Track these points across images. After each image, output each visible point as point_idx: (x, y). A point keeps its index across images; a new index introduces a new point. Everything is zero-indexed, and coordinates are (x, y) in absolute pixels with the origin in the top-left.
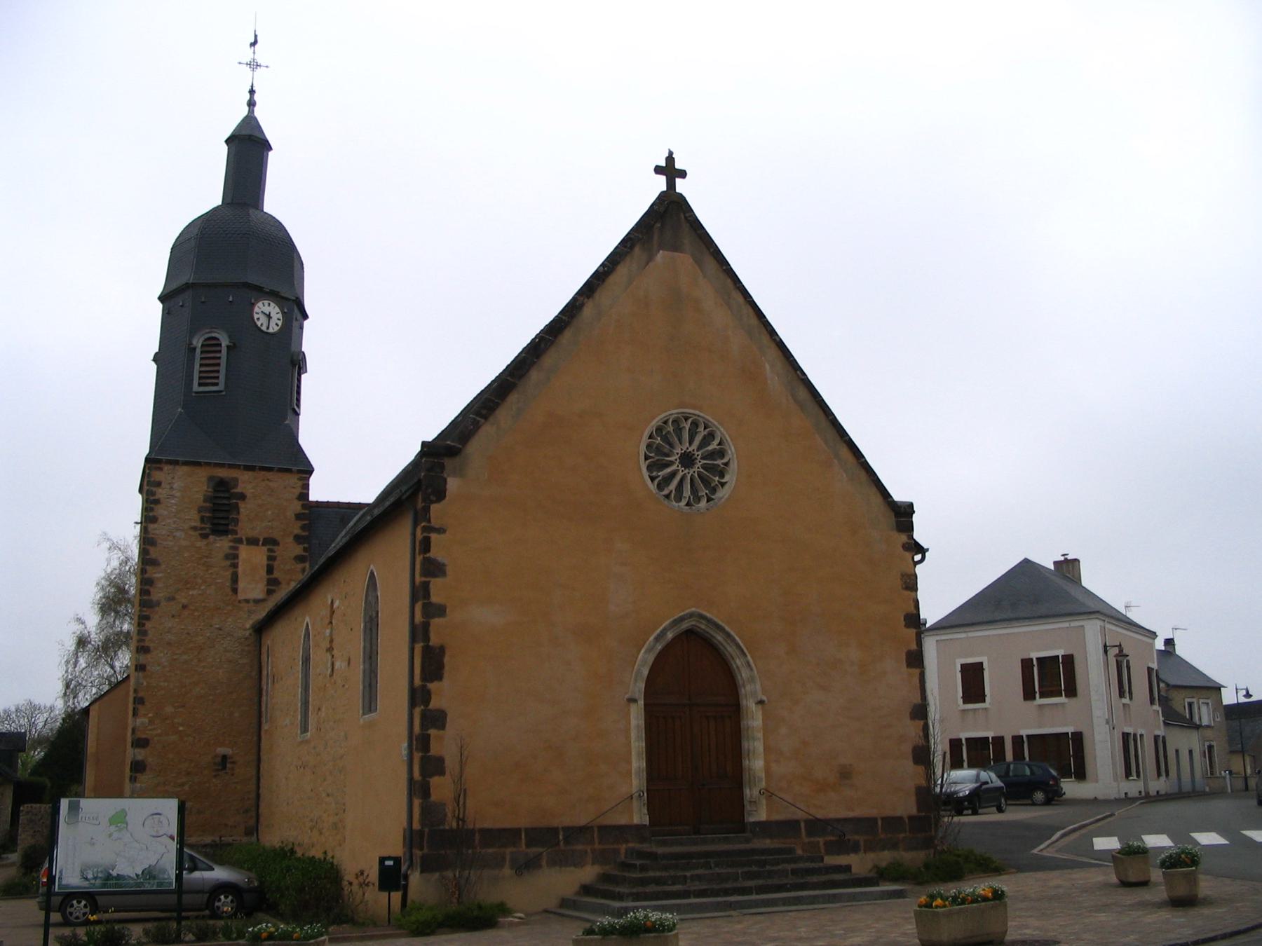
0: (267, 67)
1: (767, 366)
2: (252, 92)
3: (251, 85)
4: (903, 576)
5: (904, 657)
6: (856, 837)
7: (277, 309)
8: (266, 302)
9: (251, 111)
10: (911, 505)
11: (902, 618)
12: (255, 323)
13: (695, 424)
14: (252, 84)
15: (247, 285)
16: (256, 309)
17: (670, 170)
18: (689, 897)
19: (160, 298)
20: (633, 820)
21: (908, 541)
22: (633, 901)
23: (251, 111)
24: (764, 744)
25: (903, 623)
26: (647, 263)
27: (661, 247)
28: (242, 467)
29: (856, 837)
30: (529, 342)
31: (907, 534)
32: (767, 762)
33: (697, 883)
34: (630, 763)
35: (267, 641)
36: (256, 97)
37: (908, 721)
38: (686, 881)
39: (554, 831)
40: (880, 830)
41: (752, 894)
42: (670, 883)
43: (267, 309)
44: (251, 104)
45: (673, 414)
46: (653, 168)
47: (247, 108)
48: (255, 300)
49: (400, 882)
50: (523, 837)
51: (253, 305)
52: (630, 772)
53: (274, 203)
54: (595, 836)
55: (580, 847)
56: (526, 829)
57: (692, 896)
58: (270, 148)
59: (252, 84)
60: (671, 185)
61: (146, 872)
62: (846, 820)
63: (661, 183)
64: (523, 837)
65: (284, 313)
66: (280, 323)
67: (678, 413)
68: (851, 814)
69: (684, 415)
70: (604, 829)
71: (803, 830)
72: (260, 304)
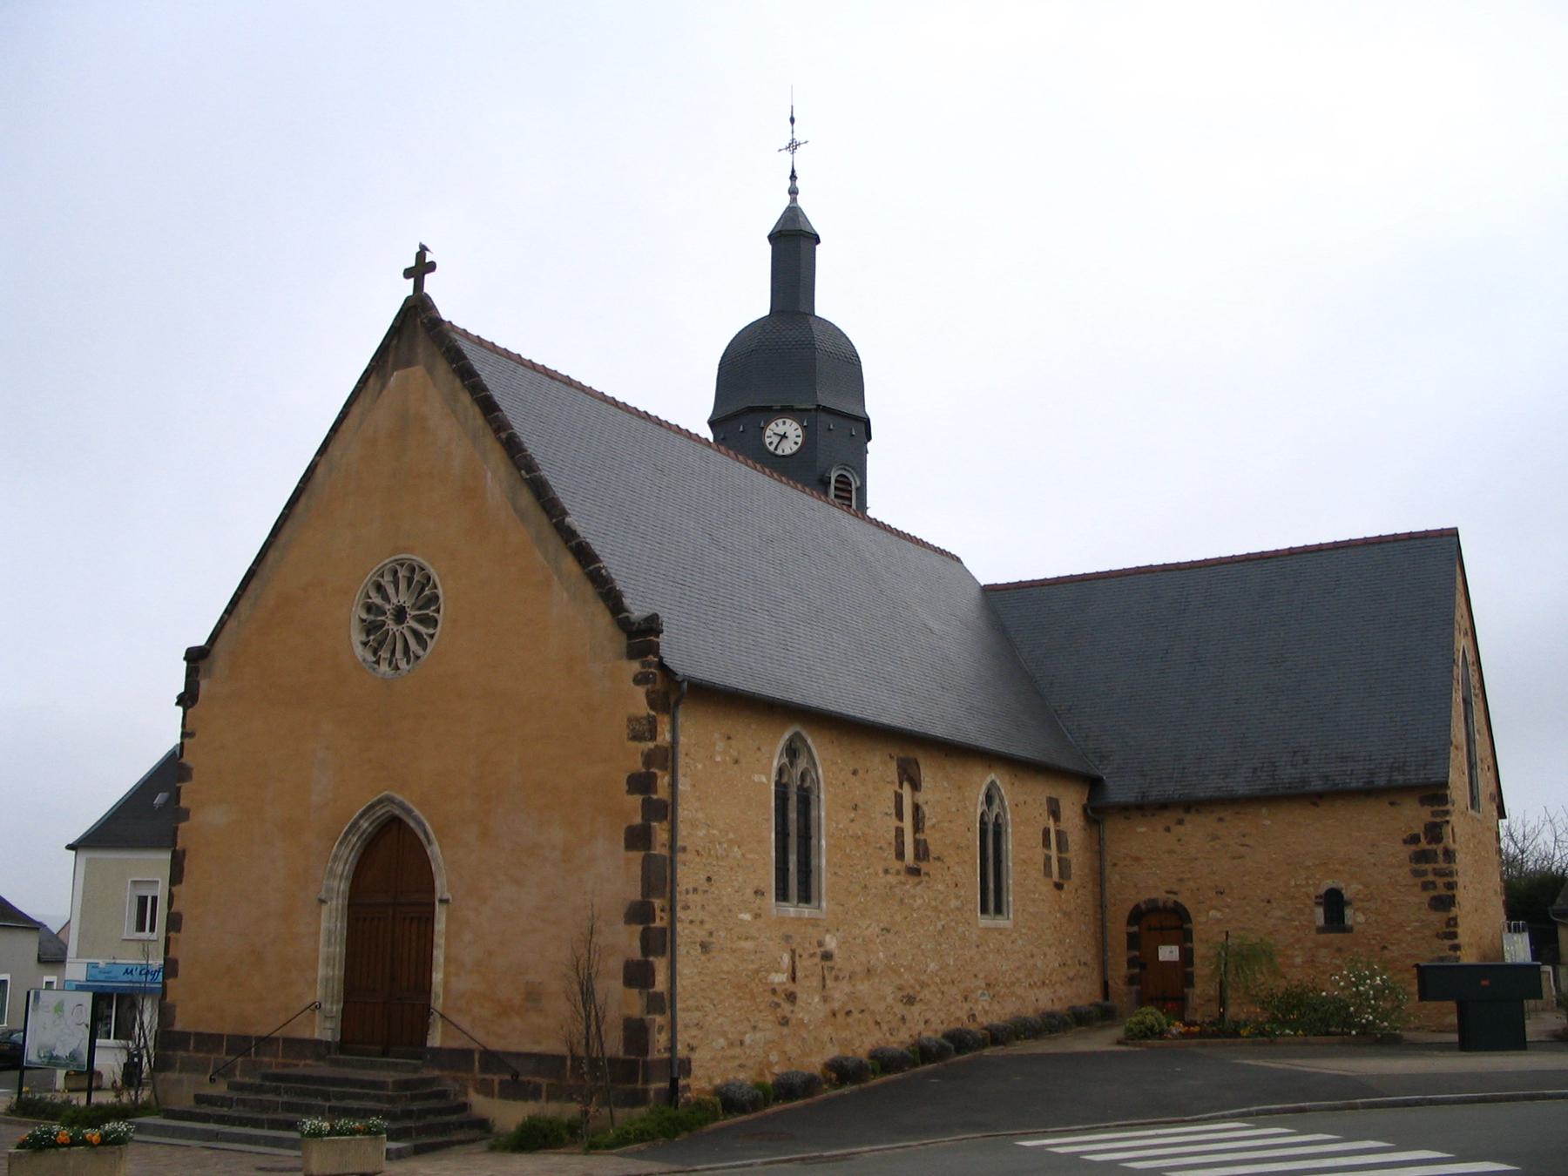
0: (780, 150)
1: (489, 475)
2: (793, 177)
4: (630, 720)
5: (623, 836)
6: (537, 1079)
7: (795, 425)
8: (780, 421)
9: (794, 200)
10: (1456, 529)
11: (625, 781)
12: (768, 448)
13: (412, 570)
14: (793, 171)
15: (751, 410)
16: (768, 433)
17: (421, 268)
18: (208, 1121)
20: (314, 1034)
21: (643, 670)
22: (164, 1118)
23: (794, 200)
24: (445, 952)
25: (625, 787)
26: (381, 392)
27: (396, 368)
29: (537, 1079)
31: (640, 660)
32: (447, 975)
33: (241, 1108)
34: (316, 970)
36: (798, 183)
37: (621, 925)
38: (232, 1105)
39: (246, 1039)
40: (568, 1074)
41: (263, 1127)
42: (219, 1104)
43: (781, 429)
44: (793, 192)
45: (385, 565)
46: (403, 271)
47: (789, 197)
48: (765, 423)
50: (225, 1044)
51: (763, 429)
52: (315, 981)
54: (280, 1048)
55: (266, 1059)
56: (228, 1036)
57: (211, 1120)
59: (793, 171)
60: (419, 286)
62: (529, 1056)
63: (408, 287)
64: (225, 1044)
65: (804, 428)
66: (800, 440)
67: (391, 562)
68: (536, 1049)
69: (399, 562)
70: (287, 1041)
71: (477, 1064)
72: (773, 426)
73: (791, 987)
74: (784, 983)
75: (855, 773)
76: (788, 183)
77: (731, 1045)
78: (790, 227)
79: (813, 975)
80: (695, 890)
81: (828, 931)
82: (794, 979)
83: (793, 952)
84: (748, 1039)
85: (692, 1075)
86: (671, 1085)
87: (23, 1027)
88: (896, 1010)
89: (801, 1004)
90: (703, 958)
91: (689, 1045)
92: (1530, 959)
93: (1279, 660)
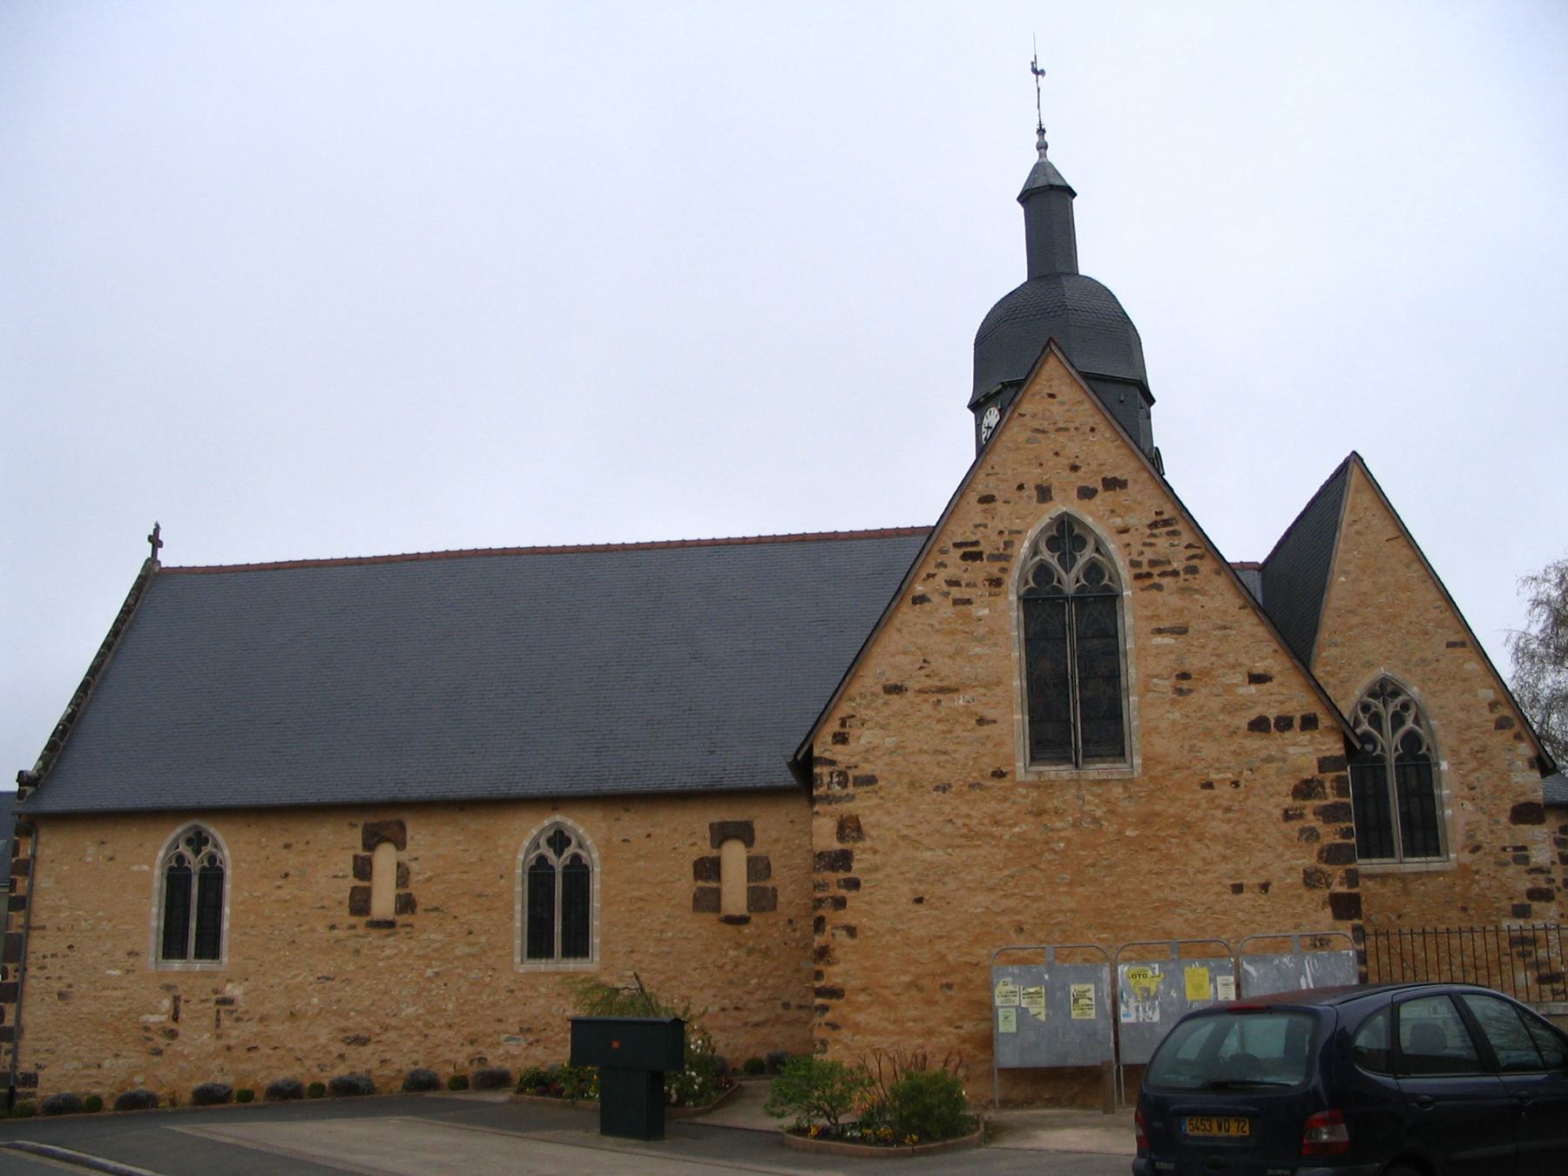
2: (1041, 131)
3: (1038, 122)
9: (1042, 155)
14: (1040, 122)
19: (969, 407)
23: (1042, 155)
28: (1364, 969)
30: (1342, 462)
35: (1446, 997)
44: (1042, 147)
47: (1037, 153)
49: (11, 962)
53: (1092, 261)
58: (1074, 194)
59: (1040, 122)
61: (697, 896)
73: (173, 1026)
74: (164, 1022)
75: (287, 846)
76: (1036, 138)
77: (87, 1067)
78: (1041, 182)
79: (205, 1016)
80: (54, 956)
81: (229, 981)
82: (175, 1018)
83: (176, 999)
84: (107, 1064)
85: (39, 1086)
86: (10, 1091)
87: (1479, 983)
88: (331, 1048)
89: (184, 1039)
90: (59, 1003)
91: (37, 1064)
92: (1128, 1062)
93: (630, 671)
